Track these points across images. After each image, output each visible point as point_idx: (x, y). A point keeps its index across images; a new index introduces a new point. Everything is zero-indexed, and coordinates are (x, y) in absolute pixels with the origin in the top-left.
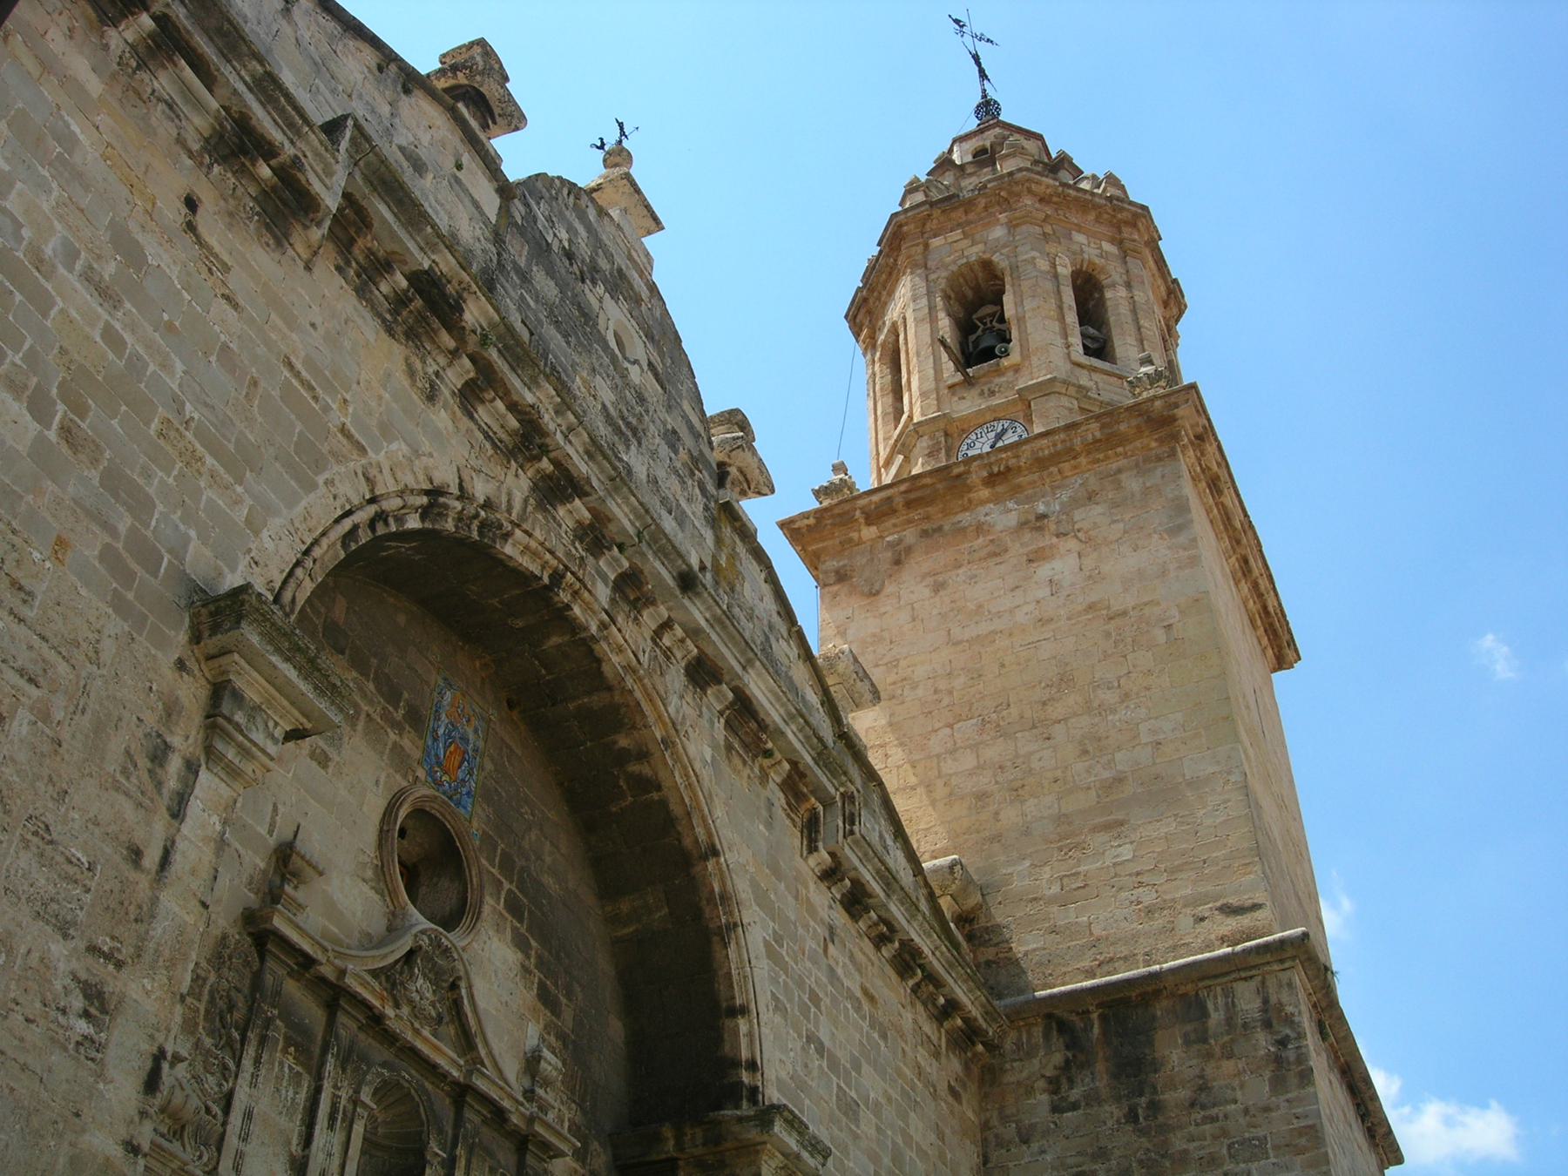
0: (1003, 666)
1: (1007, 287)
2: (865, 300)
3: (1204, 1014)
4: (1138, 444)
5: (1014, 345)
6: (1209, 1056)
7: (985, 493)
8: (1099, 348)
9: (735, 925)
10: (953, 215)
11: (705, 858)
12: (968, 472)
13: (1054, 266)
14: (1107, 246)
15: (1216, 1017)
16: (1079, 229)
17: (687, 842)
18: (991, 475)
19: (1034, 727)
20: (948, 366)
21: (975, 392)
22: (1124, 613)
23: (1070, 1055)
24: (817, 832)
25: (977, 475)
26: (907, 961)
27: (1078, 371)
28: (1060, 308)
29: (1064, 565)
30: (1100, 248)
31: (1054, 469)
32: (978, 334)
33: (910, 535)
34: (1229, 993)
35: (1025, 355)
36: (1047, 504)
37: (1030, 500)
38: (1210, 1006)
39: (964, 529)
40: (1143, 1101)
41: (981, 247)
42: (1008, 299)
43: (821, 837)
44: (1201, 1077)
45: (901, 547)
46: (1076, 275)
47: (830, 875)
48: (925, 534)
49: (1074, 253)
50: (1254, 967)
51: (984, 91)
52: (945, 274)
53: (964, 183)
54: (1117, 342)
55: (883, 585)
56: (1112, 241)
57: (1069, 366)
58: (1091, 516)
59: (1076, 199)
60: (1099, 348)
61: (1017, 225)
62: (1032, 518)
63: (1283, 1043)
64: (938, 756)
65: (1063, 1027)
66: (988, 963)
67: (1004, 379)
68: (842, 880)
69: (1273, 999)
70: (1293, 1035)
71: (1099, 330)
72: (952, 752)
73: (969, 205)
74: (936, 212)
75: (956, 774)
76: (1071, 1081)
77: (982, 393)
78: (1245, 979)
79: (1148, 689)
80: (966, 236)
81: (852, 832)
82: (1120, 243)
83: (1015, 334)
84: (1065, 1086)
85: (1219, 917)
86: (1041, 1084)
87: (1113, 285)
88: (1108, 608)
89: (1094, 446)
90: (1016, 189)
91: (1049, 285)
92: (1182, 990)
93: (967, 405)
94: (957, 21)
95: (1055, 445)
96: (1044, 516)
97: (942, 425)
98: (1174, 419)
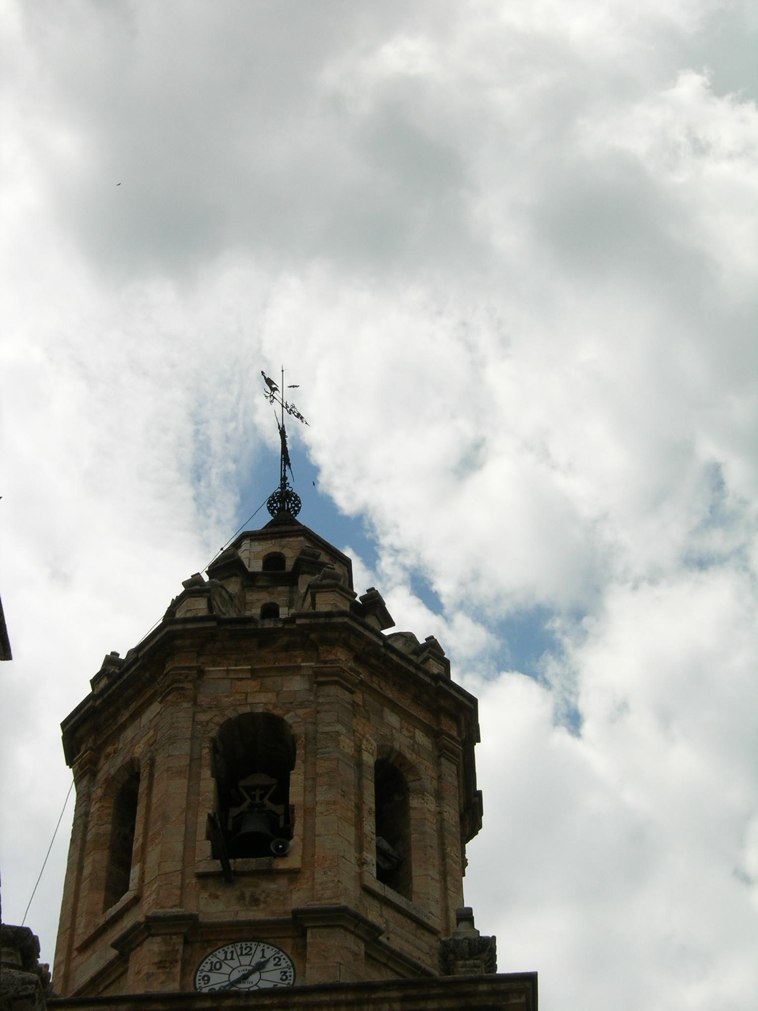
1: (298, 762)
5: (296, 843)
13: (359, 750)
14: (421, 738)
20: (205, 847)
27: (368, 901)
28: (359, 807)
30: (413, 738)
41: (270, 697)
42: (297, 779)
46: (380, 765)
51: (284, 478)
52: (219, 720)
53: (252, 597)
54: (417, 871)
57: (359, 891)
67: (273, 886)
71: (392, 843)
83: (298, 829)
87: (422, 792)
91: (350, 775)
94: (269, 382)
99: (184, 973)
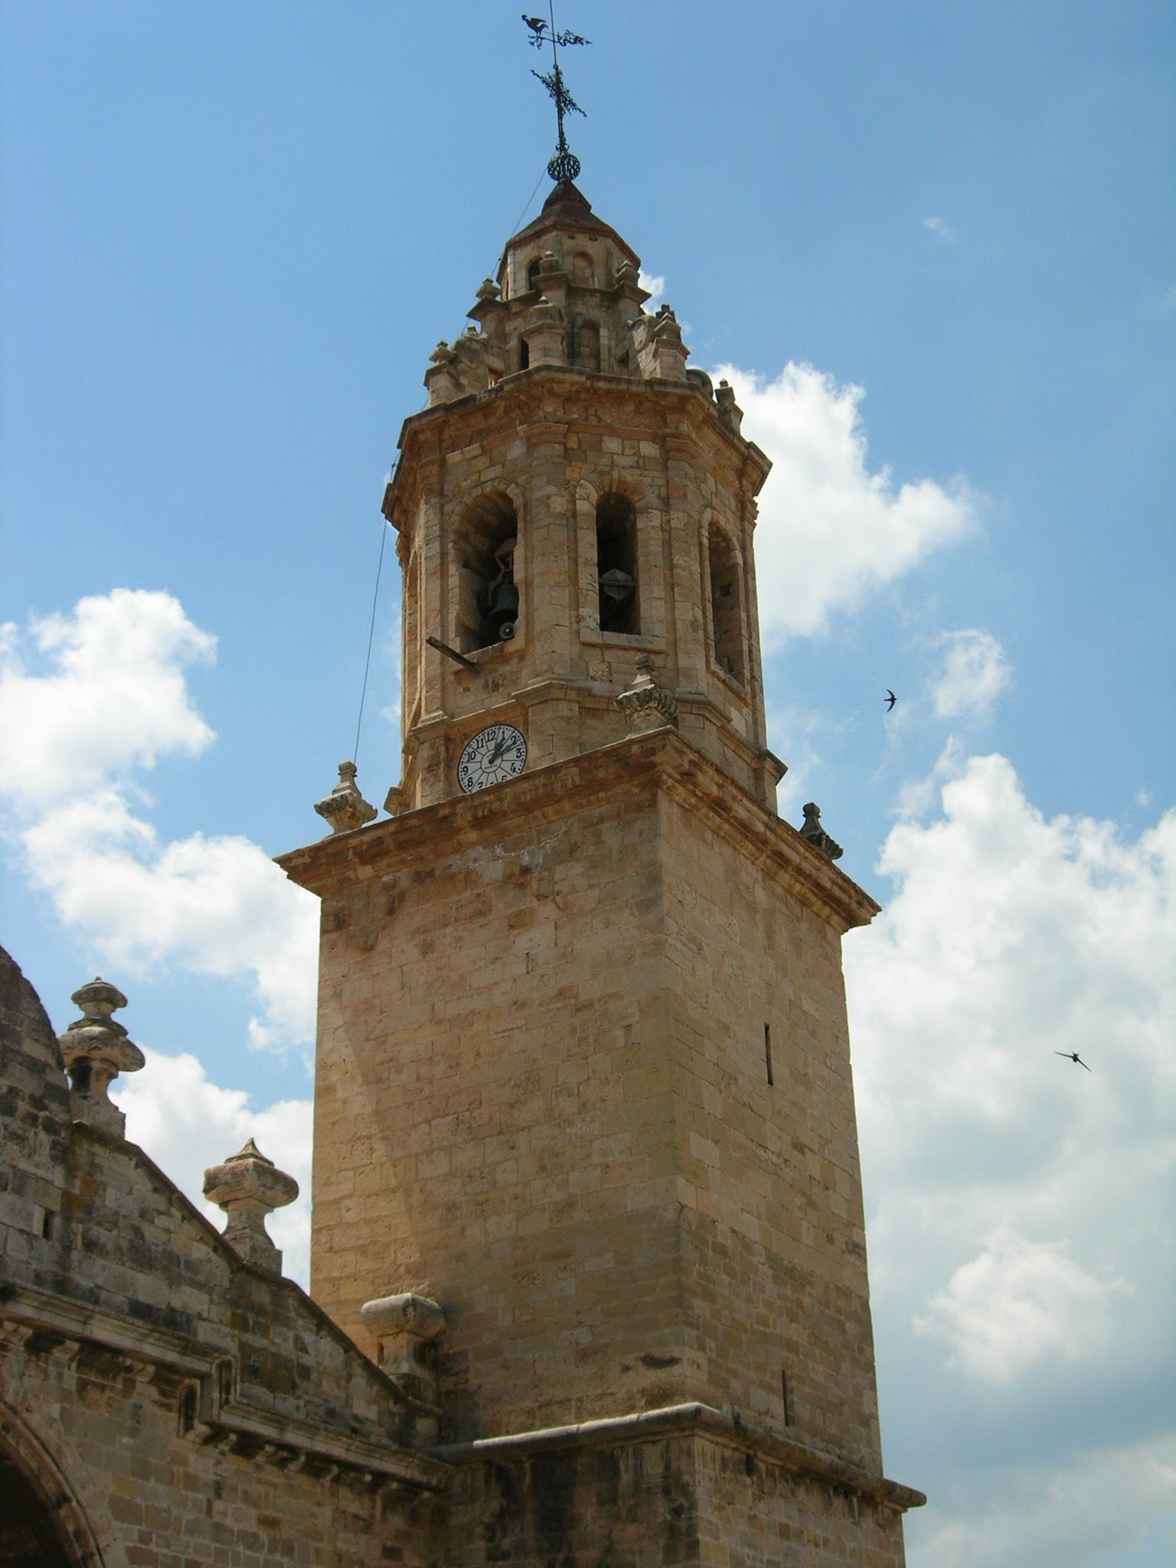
0: (478, 1055)
2: (398, 499)
3: (616, 1474)
4: (618, 789)
5: (520, 623)
6: (616, 1517)
7: (473, 836)
8: (619, 613)
9: (92, 1554)
10: (472, 421)
11: (59, 1505)
12: (453, 814)
15: (626, 1478)
16: (613, 432)
17: (41, 1495)
18: (476, 818)
19: (501, 1133)
21: (477, 685)
22: (590, 1005)
23: (504, 1503)
24: (193, 1409)
25: (462, 819)
26: (318, 1465)
29: (538, 938)
30: (637, 454)
31: (538, 813)
32: (490, 613)
33: (404, 876)
34: (638, 1455)
35: (529, 639)
36: (532, 854)
37: (516, 846)
38: (622, 1467)
39: (453, 877)
40: (561, 1557)
41: (496, 471)
43: (197, 1414)
44: (609, 1538)
45: (395, 892)
47: (217, 1433)
48: (419, 878)
49: (602, 474)
50: (660, 1433)
55: (376, 939)
56: (654, 438)
58: (570, 874)
59: (609, 392)
60: (619, 613)
61: (535, 445)
62: (516, 870)
63: (677, 1512)
64: (417, 1155)
65: (501, 1474)
66: (449, 1393)
67: (508, 668)
68: (227, 1437)
69: (674, 1466)
70: (686, 1505)
72: (429, 1153)
73: (487, 409)
74: (453, 418)
75: (431, 1179)
76: (504, 1529)
77: (486, 686)
78: (653, 1442)
79: (603, 1100)
80: (485, 451)
81: (227, 1402)
82: (660, 439)
84: (499, 1534)
85: (642, 1369)
86: (480, 1530)
88: (576, 996)
89: (572, 793)
90: (537, 392)
91: (561, 535)
92: (599, 1448)
93: (472, 703)
95: (536, 789)
96: (526, 871)
97: (442, 732)
98: (653, 765)
99: (448, 767)
